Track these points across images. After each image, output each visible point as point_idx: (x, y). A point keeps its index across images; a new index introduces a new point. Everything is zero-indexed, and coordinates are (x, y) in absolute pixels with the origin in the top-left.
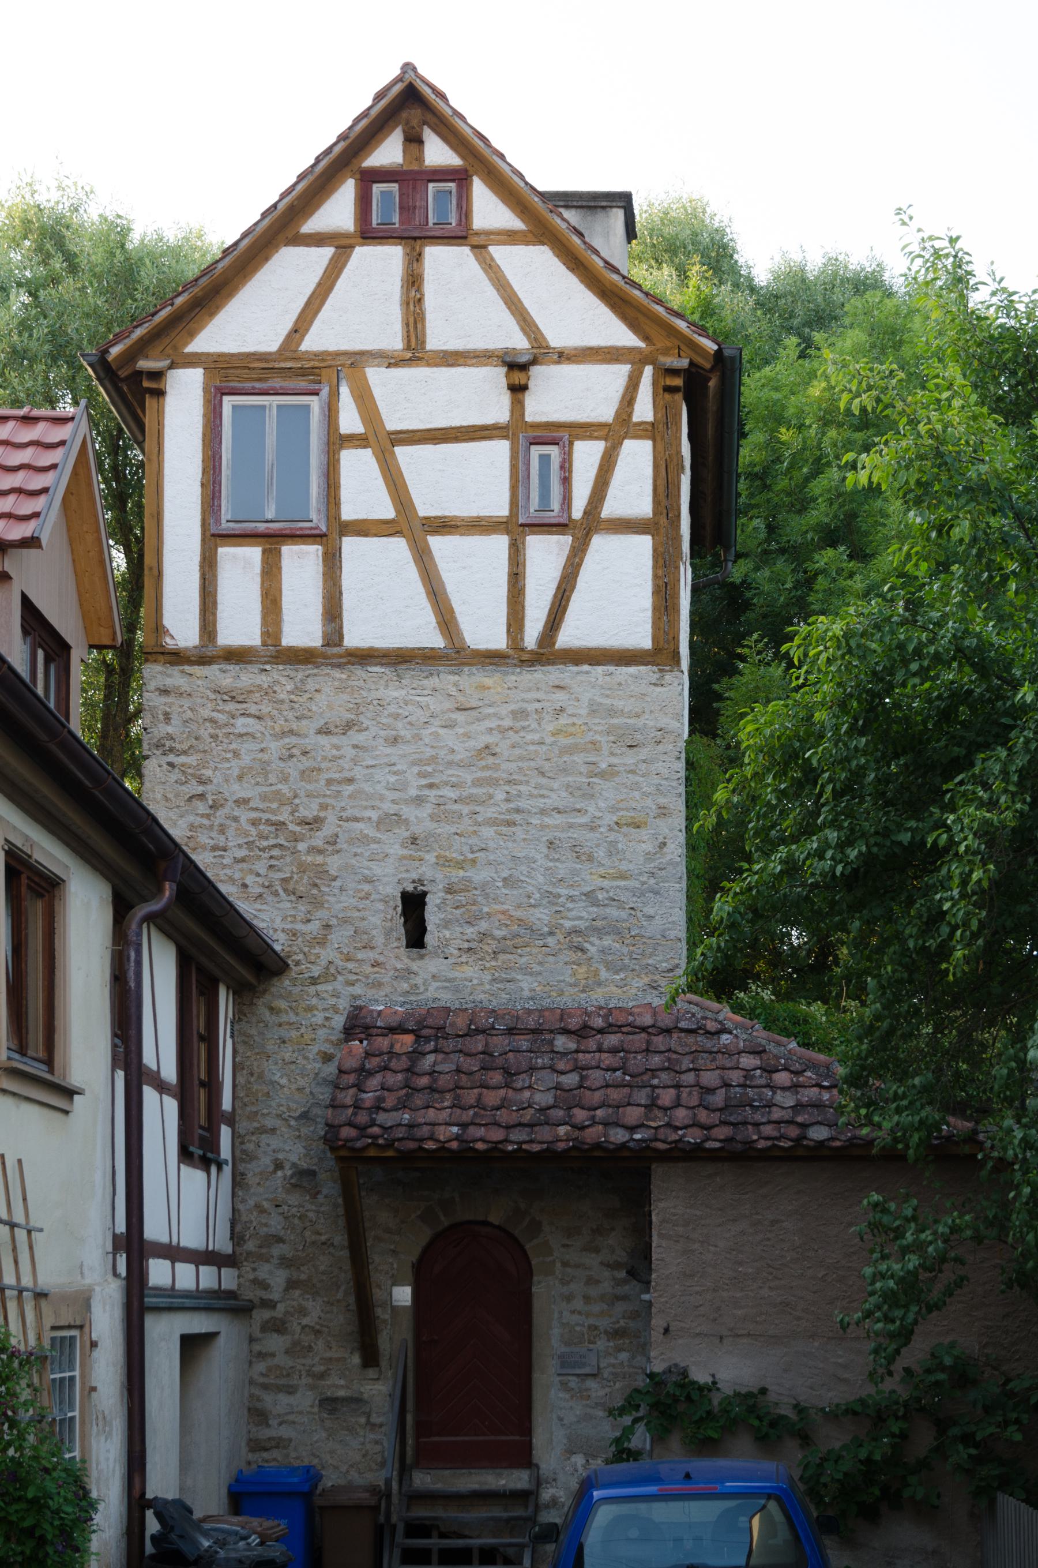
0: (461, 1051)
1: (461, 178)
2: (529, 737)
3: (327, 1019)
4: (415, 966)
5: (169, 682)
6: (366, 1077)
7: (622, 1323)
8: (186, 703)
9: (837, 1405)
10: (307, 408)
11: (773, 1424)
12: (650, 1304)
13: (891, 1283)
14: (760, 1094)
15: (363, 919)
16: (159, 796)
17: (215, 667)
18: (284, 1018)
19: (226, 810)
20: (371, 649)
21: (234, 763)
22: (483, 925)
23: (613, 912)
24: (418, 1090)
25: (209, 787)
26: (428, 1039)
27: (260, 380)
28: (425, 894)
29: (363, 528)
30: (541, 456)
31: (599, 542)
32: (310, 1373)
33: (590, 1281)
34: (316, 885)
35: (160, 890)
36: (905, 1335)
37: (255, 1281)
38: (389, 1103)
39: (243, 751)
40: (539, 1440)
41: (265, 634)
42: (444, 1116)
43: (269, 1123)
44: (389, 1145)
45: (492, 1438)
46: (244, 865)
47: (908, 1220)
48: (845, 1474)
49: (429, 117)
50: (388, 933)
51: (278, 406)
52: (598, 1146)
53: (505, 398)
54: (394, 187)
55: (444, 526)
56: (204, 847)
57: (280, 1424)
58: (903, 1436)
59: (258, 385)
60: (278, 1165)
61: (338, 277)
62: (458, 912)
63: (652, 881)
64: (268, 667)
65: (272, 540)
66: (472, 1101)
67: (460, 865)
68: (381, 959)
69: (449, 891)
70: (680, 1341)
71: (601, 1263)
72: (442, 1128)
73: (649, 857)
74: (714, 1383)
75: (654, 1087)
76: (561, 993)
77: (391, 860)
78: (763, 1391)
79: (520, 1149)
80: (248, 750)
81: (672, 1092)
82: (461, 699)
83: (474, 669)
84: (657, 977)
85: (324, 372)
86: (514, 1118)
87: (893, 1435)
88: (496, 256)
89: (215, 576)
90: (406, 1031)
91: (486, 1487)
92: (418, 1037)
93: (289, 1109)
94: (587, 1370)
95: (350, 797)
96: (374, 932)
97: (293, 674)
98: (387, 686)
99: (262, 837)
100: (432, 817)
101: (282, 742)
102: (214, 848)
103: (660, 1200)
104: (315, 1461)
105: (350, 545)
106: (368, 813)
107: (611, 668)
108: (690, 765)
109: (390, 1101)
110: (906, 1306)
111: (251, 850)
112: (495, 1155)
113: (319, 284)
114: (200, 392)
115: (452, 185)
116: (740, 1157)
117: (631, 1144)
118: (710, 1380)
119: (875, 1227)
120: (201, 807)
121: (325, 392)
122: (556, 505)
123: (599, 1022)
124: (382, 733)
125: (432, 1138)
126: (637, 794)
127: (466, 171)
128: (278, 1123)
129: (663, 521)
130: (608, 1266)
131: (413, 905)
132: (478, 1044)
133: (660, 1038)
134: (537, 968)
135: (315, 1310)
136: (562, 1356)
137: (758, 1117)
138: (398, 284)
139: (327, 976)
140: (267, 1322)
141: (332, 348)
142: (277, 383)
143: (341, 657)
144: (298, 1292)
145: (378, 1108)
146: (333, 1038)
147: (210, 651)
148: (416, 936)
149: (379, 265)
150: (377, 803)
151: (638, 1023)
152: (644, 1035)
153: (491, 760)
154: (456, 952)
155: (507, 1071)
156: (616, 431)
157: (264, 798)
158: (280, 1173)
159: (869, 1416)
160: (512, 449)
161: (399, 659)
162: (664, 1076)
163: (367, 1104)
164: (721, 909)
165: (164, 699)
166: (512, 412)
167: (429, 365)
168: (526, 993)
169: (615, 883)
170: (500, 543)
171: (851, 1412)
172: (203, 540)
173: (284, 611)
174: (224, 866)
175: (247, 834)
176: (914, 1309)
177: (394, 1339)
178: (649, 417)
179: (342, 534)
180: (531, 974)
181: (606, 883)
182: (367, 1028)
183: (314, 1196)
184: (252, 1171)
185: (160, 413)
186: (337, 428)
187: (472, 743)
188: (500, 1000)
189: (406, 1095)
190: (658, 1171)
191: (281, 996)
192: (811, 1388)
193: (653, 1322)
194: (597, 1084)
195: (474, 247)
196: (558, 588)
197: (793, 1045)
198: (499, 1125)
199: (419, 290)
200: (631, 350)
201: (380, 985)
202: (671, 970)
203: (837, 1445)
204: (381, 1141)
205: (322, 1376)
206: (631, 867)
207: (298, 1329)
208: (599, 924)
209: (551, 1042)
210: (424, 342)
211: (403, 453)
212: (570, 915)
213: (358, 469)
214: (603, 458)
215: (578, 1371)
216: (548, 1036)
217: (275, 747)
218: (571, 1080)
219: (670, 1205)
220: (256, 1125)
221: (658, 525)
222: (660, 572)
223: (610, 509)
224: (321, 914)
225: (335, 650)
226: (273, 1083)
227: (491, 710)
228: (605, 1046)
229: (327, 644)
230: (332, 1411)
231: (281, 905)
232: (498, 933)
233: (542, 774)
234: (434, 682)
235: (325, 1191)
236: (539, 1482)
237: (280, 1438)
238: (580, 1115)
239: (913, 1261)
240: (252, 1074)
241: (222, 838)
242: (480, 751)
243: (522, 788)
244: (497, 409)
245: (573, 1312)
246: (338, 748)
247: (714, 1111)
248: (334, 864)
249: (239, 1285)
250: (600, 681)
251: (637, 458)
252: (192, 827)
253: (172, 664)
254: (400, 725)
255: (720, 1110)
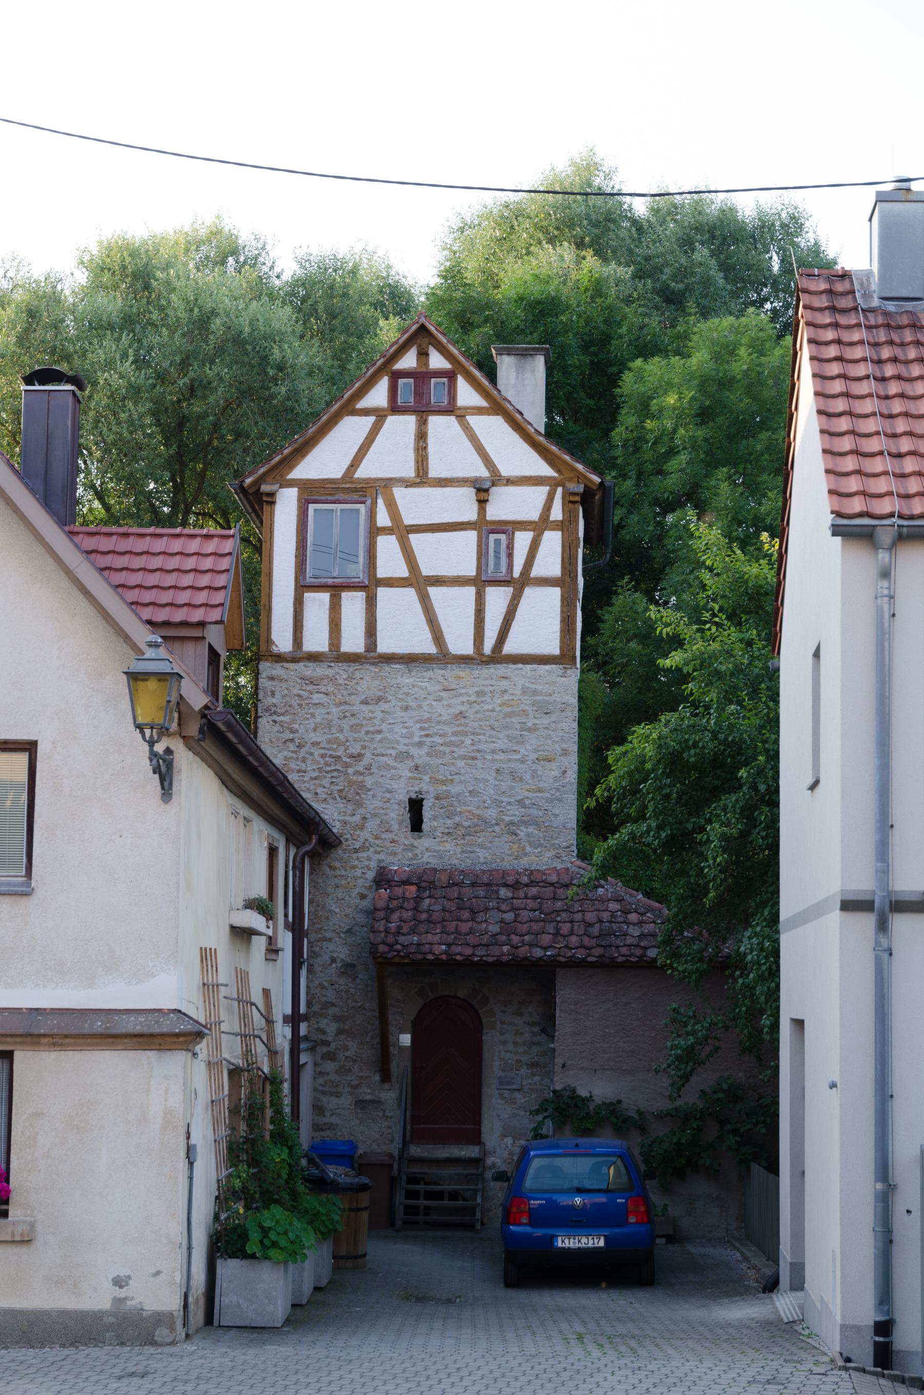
0: (444, 897)
1: (451, 376)
2: (486, 707)
3: (363, 873)
4: (416, 843)
5: (274, 673)
6: (391, 913)
7: (536, 1059)
8: (284, 685)
9: (662, 1111)
10: (358, 511)
11: (624, 1121)
12: (554, 1050)
13: (679, 1051)
14: (619, 928)
15: (386, 814)
16: (267, 740)
17: (302, 664)
18: (338, 873)
19: (306, 749)
20: (393, 654)
21: (311, 721)
22: (457, 819)
23: (534, 812)
24: (421, 922)
25: (296, 735)
26: (425, 889)
27: (330, 494)
28: (422, 800)
29: (390, 583)
30: (495, 540)
31: (528, 591)
32: (349, 1085)
33: (518, 1033)
34: (358, 794)
35: (311, 839)
36: (686, 1078)
37: (318, 1029)
38: (405, 930)
39: (316, 714)
40: (485, 1128)
41: (331, 645)
42: (437, 938)
43: (328, 935)
44: (407, 956)
45: (457, 1126)
46: (316, 782)
47: (690, 1018)
48: (665, 1151)
49: (432, 340)
50: (400, 823)
51: (341, 510)
52: (526, 959)
53: (475, 507)
54: (411, 381)
55: (438, 581)
56: (293, 771)
57: (331, 1115)
58: (699, 1129)
59: (329, 498)
60: (333, 960)
61: (377, 434)
62: (442, 811)
63: (558, 794)
64: (332, 664)
65: (336, 590)
66: (453, 930)
67: (444, 783)
68: (396, 838)
69: (437, 798)
70: (572, 1072)
71: (524, 1022)
72: (436, 946)
73: (556, 779)
74: (591, 1097)
75: (558, 922)
76: (503, 860)
77: (403, 779)
78: (619, 1102)
79: (481, 960)
80: (320, 713)
81: (569, 925)
82: (446, 684)
83: (454, 667)
84: (560, 851)
85: (368, 490)
86: (477, 941)
87: (694, 1129)
88: (470, 422)
89: (302, 610)
90: (412, 884)
91: (454, 1156)
92: (419, 887)
93: (340, 927)
94: (514, 1087)
95: (379, 741)
96: (392, 822)
97: (347, 669)
98: (402, 676)
99: (327, 764)
100: (428, 754)
101: (339, 709)
102: (299, 771)
103: (561, 990)
104: (352, 1138)
105: (382, 592)
106: (389, 752)
107: (535, 666)
108: (580, 698)
109: (405, 929)
110: (687, 1063)
111: (320, 772)
112: (467, 963)
113: (366, 438)
114: (296, 502)
115: (445, 380)
116: (608, 966)
117: (545, 958)
118: (588, 1095)
119: (673, 1021)
120: (292, 747)
121: (369, 502)
122: (504, 569)
123: (525, 880)
124: (399, 704)
125: (431, 952)
126: (549, 742)
127: (454, 372)
128: (334, 935)
129: (567, 579)
130: (528, 1024)
131: (416, 806)
132: (454, 892)
133: (562, 890)
134: (488, 845)
135: (353, 1047)
136: (500, 1078)
137: (618, 942)
138: (413, 438)
139: (364, 848)
140: (325, 1054)
141: (374, 476)
142: (340, 496)
143: (375, 658)
144: (343, 1037)
145: (398, 933)
146: (367, 885)
147: (298, 654)
148: (417, 825)
149: (401, 427)
150: (395, 745)
151: (548, 880)
152: (552, 888)
153: (463, 720)
154: (440, 835)
155: (472, 911)
156: (539, 526)
157: (329, 742)
158: (334, 965)
159: (680, 1117)
160: (478, 536)
161: (410, 660)
162: (564, 915)
163: (393, 931)
164: (597, 859)
165: (270, 683)
166: (479, 514)
167: (430, 486)
168: (482, 860)
169: (536, 795)
170: (471, 591)
171: (668, 1114)
172: (296, 589)
173: (343, 631)
174: (304, 782)
175: (318, 763)
176: (691, 1064)
177: (400, 1065)
178: (560, 518)
179: (377, 586)
180: (485, 848)
181: (530, 795)
182: (389, 881)
183: (354, 979)
184: (318, 963)
185: (272, 514)
186: (375, 523)
187: (452, 711)
188: (466, 864)
189: (415, 925)
190: (560, 972)
191: (336, 860)
192: (647, 1101)
193: (556, 1060)
194: (525, 920)
195: (457, 416)
196: (505, 618)
197: (640, 896)
198: (469, 945)
199: (425, 441)
200: (550, 478)
201: (395, 854)
202: (568, 847)
203: (661, 1134)
204: (402, 954)
205: (356, 1087)
206: (545, 785)
207: (343, 1059)
208: (526, 819)
209: (497, 892)
210: (427, 473)
211: (413, 538)
212: (508, 813)
213: (387, 546)
214: (532, 541)
215: (509, 1087)
216: (495, 888)
217: (335, 711)
218: (509, 916)
219: (566, 993)
220: (320, 936)
221: (565, 581)
222: (565, 609)
223: (536, 572)
224: (361, 811)
225: (372, 654)
226: (330, 911)
227: (463, 691)
228: (529, 895)
229: (367, 651)
230: (363, 1108)
231: (338, 805)
232: (466, 824)
233: (493, 729)
234: (430, 674)
235: (361, 976)
236: (485, 1153)
237: (331, 1124)
238: (515, 939)
239: (691, 1040)
240: (318, 906)
241: (304, 765)
242: (456, 716)
243: (482, 737)
244: (470, 513)
245: (507, 1052)
246: (373, 712)
247: (593, 938)
248: (369, 781)
249: (309, 1032)
250: (529, 674)
251: (552, 541)
252: (286, 758)
253: (276, 662)
254: (409, 699)
255: (596, 937)
